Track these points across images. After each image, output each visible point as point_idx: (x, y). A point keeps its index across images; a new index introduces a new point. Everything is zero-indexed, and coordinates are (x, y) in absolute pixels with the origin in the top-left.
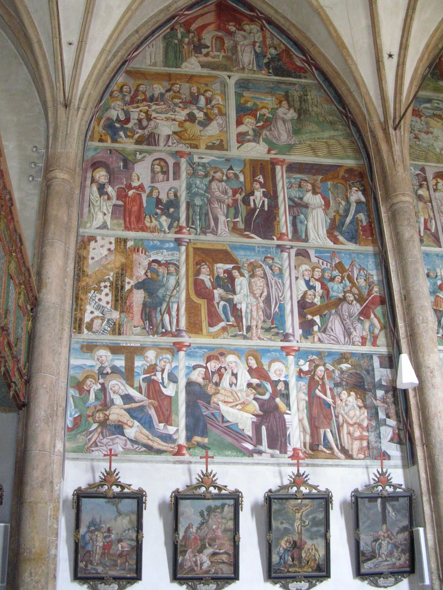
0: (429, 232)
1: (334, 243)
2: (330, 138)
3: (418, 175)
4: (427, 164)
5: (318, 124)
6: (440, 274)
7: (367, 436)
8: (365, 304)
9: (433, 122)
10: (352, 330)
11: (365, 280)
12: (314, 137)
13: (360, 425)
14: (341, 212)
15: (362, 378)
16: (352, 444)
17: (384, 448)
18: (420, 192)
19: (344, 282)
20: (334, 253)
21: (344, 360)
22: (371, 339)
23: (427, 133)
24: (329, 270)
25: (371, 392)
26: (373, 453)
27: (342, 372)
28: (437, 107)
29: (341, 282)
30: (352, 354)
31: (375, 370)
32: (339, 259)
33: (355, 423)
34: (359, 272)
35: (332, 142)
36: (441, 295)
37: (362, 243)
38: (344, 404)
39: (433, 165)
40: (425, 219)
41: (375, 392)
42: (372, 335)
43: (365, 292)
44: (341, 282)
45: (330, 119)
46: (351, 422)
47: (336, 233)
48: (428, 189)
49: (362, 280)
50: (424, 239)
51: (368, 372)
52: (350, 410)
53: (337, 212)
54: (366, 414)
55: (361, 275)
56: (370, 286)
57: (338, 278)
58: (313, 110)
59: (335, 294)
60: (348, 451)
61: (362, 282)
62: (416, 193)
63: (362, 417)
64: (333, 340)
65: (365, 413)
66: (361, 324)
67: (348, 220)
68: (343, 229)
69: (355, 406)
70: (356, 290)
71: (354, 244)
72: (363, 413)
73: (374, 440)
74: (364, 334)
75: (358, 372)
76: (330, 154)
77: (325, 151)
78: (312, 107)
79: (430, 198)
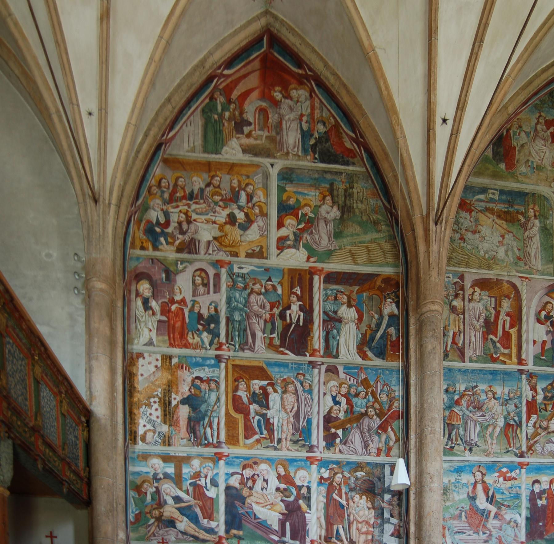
0: (456, 346)
2: (373, 241)
3: (455, 283)
5: (361, 224)
11: (387, 396)
12: (354, 241)
13: (367, 523)
14: (373, 326)
15: (374, 484)
16: (359, 537)
18: (455, 303)
20: (361, 369)
21: (360, 469)
23: (474, 232)
24: (355, 386)
27: (357, 479)
29: (365, 398)
30: (368, 464)
31: (386, 477)
33: (364, 521)
34: (383, 388)
35: (373, 246)
37: (389, 359)
38: (356, 506)
39: (474, 271)
41: (384, 496)
43: (386, 407)
44: (365, 398)
46: (360, 520)
47: (366, 349)
48: (463, 300)
49: (385, 396)
51: (379, 479)
53: (369, 326)
56: (391, 401)
57: (363, 394)
58: (357, 207)
59: (358, 409)
62: (450, 304)
63: (370, 516)
64: (352, 451)
66: (379, 437)
67: (379, 335)
68: (373, 344)
69: (365, 507)
72: (371, 513)
74: (380, 445)
76: (370, 262)
77: (365, 257)
78: (357, 203)
79: (464, 310)
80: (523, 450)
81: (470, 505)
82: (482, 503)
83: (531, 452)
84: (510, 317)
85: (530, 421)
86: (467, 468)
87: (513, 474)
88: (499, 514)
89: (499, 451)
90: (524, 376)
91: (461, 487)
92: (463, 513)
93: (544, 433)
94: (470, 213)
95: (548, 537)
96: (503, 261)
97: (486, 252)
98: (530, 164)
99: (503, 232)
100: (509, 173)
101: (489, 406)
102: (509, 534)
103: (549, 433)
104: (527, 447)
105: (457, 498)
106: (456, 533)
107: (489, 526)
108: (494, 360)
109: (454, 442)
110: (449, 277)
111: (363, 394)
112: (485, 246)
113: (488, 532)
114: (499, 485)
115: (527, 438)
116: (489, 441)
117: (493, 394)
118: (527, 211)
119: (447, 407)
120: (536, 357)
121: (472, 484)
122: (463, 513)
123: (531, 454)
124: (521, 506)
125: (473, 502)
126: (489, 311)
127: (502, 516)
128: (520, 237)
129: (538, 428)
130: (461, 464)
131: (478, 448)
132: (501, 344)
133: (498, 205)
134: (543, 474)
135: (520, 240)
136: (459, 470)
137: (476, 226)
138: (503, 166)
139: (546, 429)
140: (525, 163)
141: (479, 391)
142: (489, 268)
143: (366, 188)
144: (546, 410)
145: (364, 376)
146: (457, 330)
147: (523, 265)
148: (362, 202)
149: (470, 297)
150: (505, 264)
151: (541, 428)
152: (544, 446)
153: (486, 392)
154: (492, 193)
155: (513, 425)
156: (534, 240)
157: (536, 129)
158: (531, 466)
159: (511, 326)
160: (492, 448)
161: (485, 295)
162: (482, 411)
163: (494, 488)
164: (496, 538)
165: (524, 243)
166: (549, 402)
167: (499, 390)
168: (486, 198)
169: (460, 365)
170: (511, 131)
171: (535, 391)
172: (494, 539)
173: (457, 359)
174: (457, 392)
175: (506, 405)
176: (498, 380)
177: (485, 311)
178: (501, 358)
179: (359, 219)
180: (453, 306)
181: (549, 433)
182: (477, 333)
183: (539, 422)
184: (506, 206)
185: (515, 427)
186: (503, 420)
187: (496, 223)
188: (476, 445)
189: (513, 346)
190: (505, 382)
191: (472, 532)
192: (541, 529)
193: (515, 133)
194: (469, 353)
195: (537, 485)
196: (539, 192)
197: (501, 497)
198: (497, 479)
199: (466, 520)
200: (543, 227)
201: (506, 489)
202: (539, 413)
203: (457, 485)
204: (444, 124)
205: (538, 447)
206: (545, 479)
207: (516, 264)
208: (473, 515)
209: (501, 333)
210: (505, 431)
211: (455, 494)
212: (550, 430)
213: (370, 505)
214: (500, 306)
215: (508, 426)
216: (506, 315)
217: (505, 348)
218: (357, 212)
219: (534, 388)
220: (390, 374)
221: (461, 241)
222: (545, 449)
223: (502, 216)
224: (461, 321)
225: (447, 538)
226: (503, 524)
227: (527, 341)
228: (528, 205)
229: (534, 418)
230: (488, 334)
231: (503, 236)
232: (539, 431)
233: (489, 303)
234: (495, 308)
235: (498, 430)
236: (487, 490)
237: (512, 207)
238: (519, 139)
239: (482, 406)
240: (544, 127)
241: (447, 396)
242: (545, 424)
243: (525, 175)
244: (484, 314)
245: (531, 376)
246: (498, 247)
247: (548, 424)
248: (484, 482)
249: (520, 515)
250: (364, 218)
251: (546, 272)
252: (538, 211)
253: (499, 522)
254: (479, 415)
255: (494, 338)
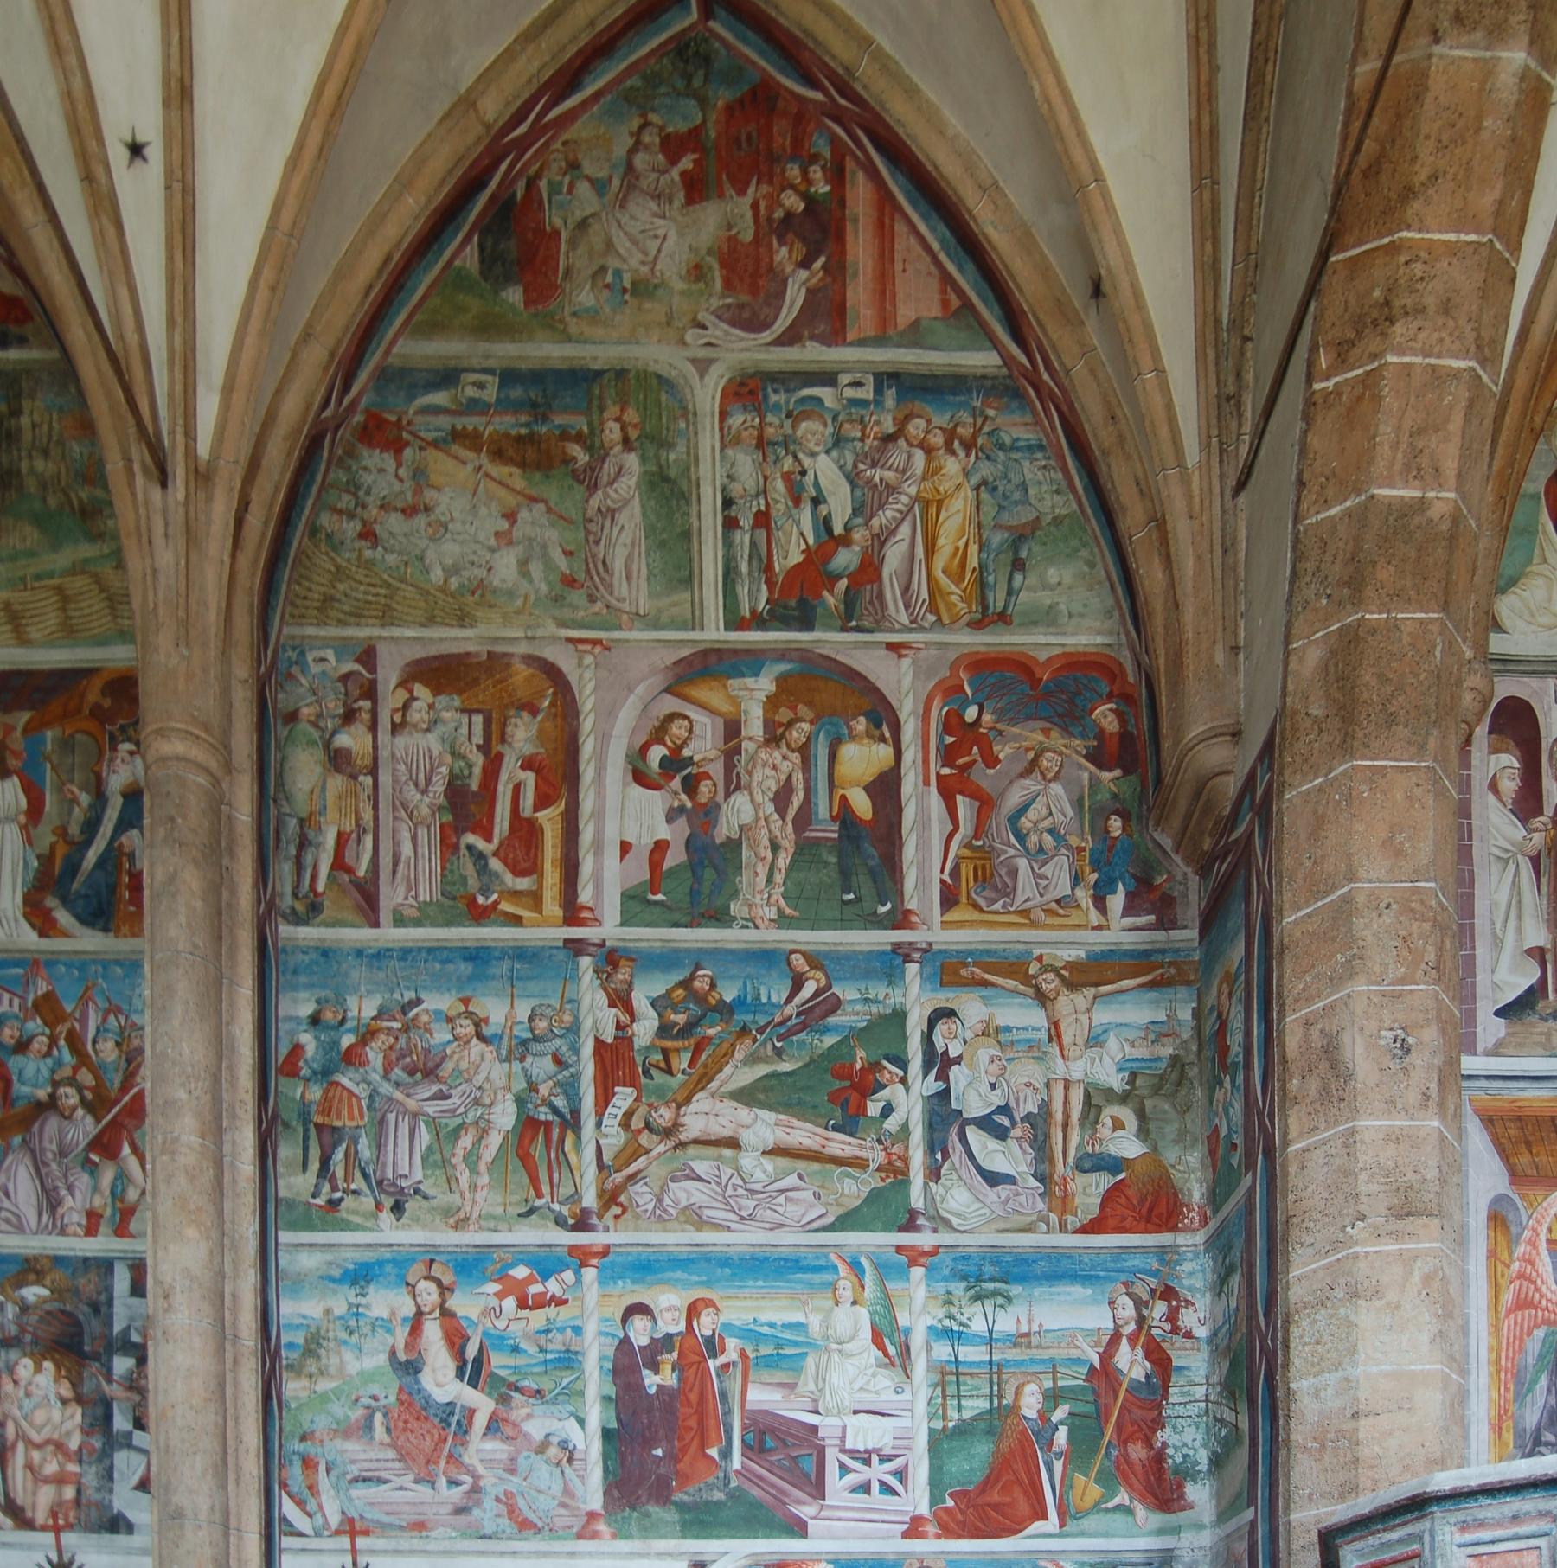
0: (346, 878)
1: (42, 934)
2: (75, 570)
3: (345, 678)
4: (385, 633)
5: (39, 520)
6: (355, 1013)
7: (76, 1474)
8: (109, 1117)
9: (438, 462)
10: (63, 1192)
11: (118, 1044)
12: (22, 573)
13: (60, 1447)
14: (74, 830)
15: (78, 1324)
16: (34, 1493)
17: (118, 1504)
18: (343, 740)
19: (55, 1052)
20: (35, 964)
21: (32, 1277)
22: (114, 1215)
23: (409, 512)
24: (17, 1017)
25: (98, 1360)
26: (88, 1515)
27: (25, 1308)
28: (473, 402)
29: (48, 1054)
30: (58, 1260)
31: (116, 1302)
32: (49, 983)
33: (48, 1442)
34: (105, 1019)
35: (79, 583)
36: (345, 1081)
37: (125, 929)
38: (22, 1393)
39: (409, 633)
40: (340, 834)
41: (110, 1361)
42: (118, 1205)
43: (116, 1080)
44: (48, 1054)
45: (83, 495)
46: (37, 1438)
47: (51, 902)
48: (373, 727)
49: (110, 1045)
50: (326, 903)
51: (95, 1308)
52: (35, 1408)
53: (62, 832)
54: (78, 1418)
55: (106, 1030)
56: (129, 1062)
57: (40, 1043)
58: (32, 470)
59: (26, 1090)
60: (22, 1509)
61: (108, 1052)
62: (327, 744)
63: (68, 1425)
64: (7, 1221)
65: (77, 1414)
66: (92, 1174)
67: (92, 856)
68: (75, 886)
69: (52, 1398)
70: (90, 1077)
71: (100, 934)
72: (72, 1416)
73: (95, 1483)
74: (98, 1202)
75: (68, 1307)
76: (69, 632)
77: (52, 620)
78: (30, 457)
79: (375, 759)
80: (585, 1204)
81: (401, 1390)
82: (441, 1381)
83: (617, 1210)
84: (538, 772)
85: (610, 1110)
86: (388, 1268)
87: (553, 1287)
88: (505, 1420)
89: (500, 1210)
90: (585, 962)
91: (366, 1329)
92: (378, 1417)
93: (661, 1148)
94: (398, 452)
95: (686, 1498)
96: (511, 594)
97: (454, 570)
98: (609, 279)
99: (512, 500)
100: (536, 315)
101: (464, 1065)
102: (543, 1487)
103: (682, 1145)
104: (601, 1194)
105: (353, 1366)
106: (356, 1480)
107: (470, 1457)
108: (480, 915)
109: (341, 1184)
110: (323, 660)
111: (40, 1043)
112: (450, 550)
113: (468, 1479)
114: (501, 1324)
115: (601, 1166)
116: (465, 1178)
117: (477, 1025)
118: (596, 429)
119: (315, 1073)
120: (628, 897)
121: (405, 1320)
122: (378, 1417)
123: (617, 1217)
124: (582, 1393)
125: (409, 1379)
126: (464, 757)
127: (515, 1425)
128: (573, 514)
129: (639, 1131)
130: (368, 1256)
131: (425, 1204)
132: (505, 862)
133: (497, 419)
134: (661, 1282)
135: (570, 522)
136: (360, 1276)
137: (418, 491)
138: (514, 295)
139: (668, 1132)
140: (594, 277)
141: (425, 1018)
142: (463, 619)
143: (61, 410)
144: (669, 1071)
145: (42, 987)
146: (349, 825)
147: (584, 601)
148: (45, 453)
149: (398, 718)
150: (519, 602)
151: (651, 1131)
152: (663, 1189)
153: (450, 1020)
154: (474, 384)
155: (548, 1124)
156: (622, 518)
157: (630, 167)
158: (619, 1259)
159: (542, 802)
160: (474, 1202)
161: (449, 708)
162: (439, 1080)
163: (485, 1333)
164: (498, 1500)
165: (588, 532)
166: (679, 1044)
167: (495, 1011)
168: (455, 399)
169: (363, 935)
170: (543, 184)
171: (628, 1008)
172: (488, 1503)
173: (349, 916)
174: (349, 1024)
175: (522, 1059)
176: (493, 978)
177: (448, 758)
178: (505, 906)
179: (37, 505)
180: (337, 751)
181: (682, 1145)
182: (422, 833)
183: (643, 1110)
184: (523, 419)
185: (556, 1131)
186: (512, 1109)
187: (487, 475)
188: (417, 1191)
189: (548, 866)
190: (518, 984)
191: (411, 1477)
192: (662, 1471)
193: (554, 189)
194: (391, 896)
195: (639, 1325)
196: (640, 365)
197: (511, 1361)
198: (494, 1302)
199: (387, 1440)
200: (653, 474)
201: (526, 1336)
202: (643, 1080)
203: (353, 1323)
204: (138, 162)
205: (642, 1195)
206: (669, 1303)
207: (558, 600)
208: (413, 1424)
209: (506, 824)
210: (520, 1145)
211: (348, 1356)
212: (683, 1137)
213: (66, 1390)
214: (503, 739)
215: (528, 1126)
216: (523, 767)
217: (518, 872)
218: (31, 485)
219: (621, 1000)
220: (126, 976)
221: (363, 543)
222: (667, 1201)
223: (511, 452)
224: (363, 796)
225: (324, 1498)
226: (518, 1452)
227: (598, 846)
228: (602, 409)
229: (624, 1098)
230: (459, 831)
231: (511, 517)
232: (645, 1139)
233: (464, 730)
234: (484, 748)
235: (495, 1140)
236: (458, 1341)
237: (545, 419)
238: (568, 206)
239: (438, 1066)
240: (661, 157)
241: (317, 1038)
242: (664, 1115)
243: (593, 316)
244: (444, 770)
245: (611, 959)
246: (492, 550)
247: (678, 1115)
248: (446, 1314)
249: (581, 1422)
250: (52, 501)
251: (664, 618)
252: (635, 426)
253: (505, 1447)
254: (427, 1095)
255: (481, 844)
